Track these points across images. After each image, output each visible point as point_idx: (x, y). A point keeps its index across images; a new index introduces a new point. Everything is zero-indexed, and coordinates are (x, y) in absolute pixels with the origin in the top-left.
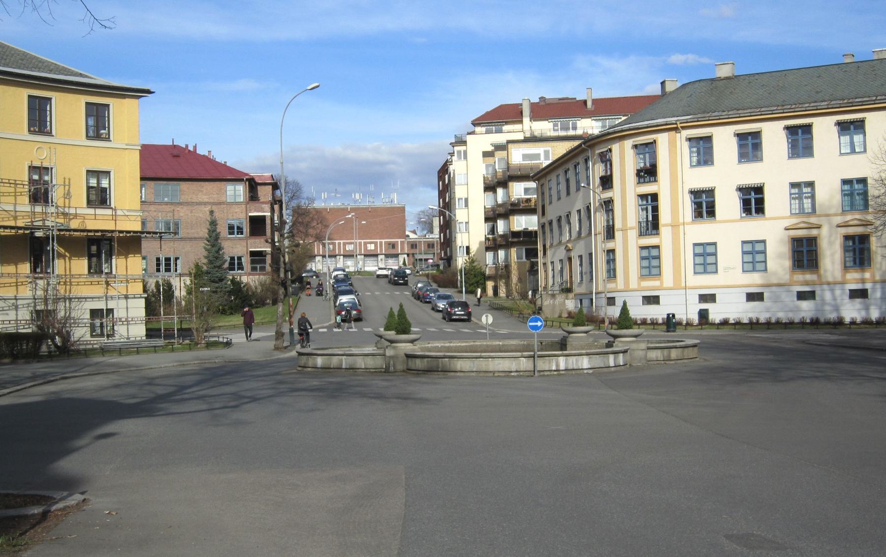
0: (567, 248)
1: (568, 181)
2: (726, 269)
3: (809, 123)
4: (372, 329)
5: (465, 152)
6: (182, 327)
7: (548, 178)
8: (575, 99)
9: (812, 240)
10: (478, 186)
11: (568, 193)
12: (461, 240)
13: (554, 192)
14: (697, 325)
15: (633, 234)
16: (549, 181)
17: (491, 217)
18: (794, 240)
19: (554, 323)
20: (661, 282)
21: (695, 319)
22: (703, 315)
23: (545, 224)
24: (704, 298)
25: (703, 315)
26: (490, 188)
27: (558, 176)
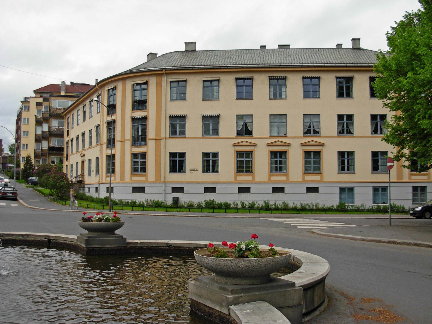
0: (82, 155)
1: (84, 113)
2: (192, 171)
3: (251, 77)
4: (6, 204)
5: (29, 107)
6: (132, 208)
7: (72, 113)
8: (122, 236)
9: (249, 153)
10: (33, 121)
11: (84, 120)
12: (24, 154)
13: (75, 121)
14: (196, 208)
15: (128, 144)
16: (72, 115)
17: (38, 140)
18: (237, 153)
19: (65, 204)
20: (146, 178)
21: (170, 202)
22: (176, 201)
23: (68, 141)
24: (175, 190)
25: (176, 201)
26: (39, 123)
27: (78, 111)
